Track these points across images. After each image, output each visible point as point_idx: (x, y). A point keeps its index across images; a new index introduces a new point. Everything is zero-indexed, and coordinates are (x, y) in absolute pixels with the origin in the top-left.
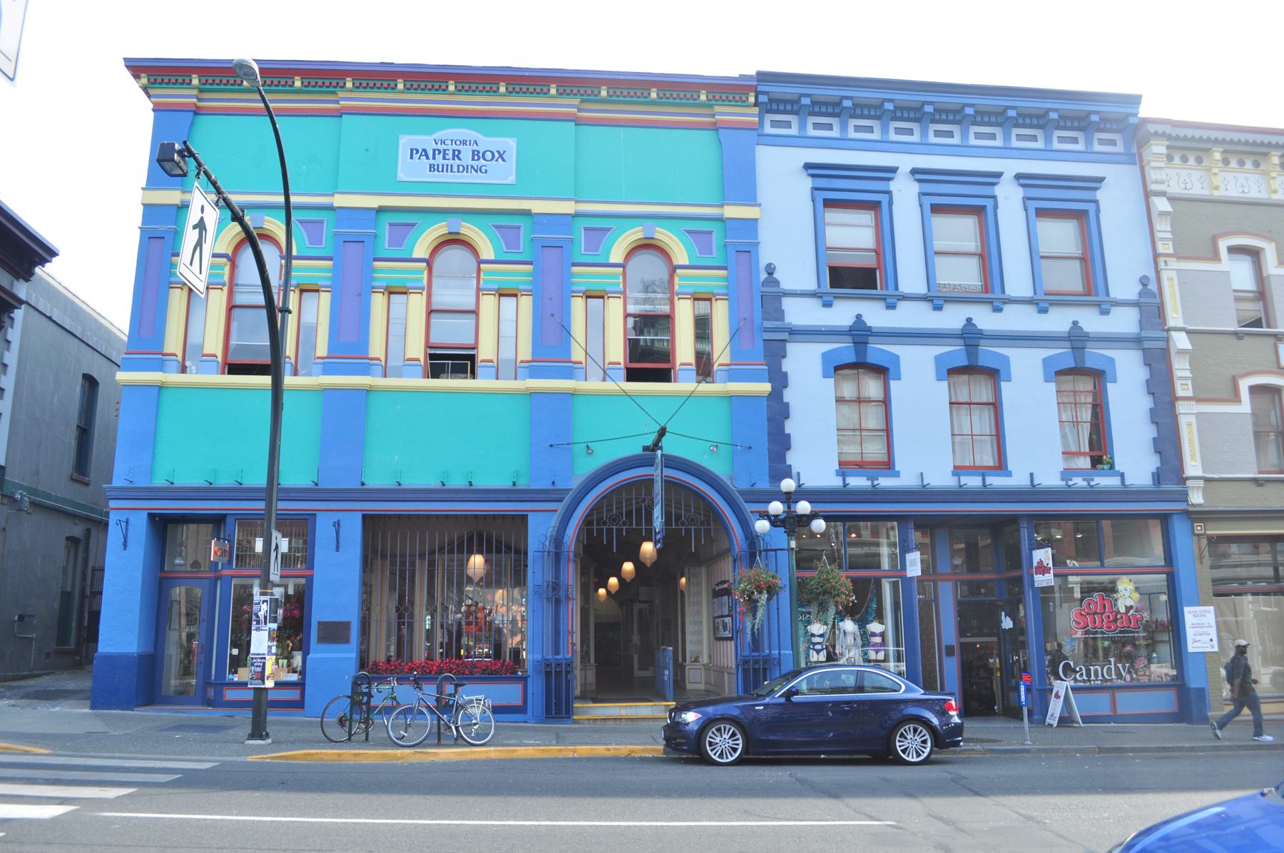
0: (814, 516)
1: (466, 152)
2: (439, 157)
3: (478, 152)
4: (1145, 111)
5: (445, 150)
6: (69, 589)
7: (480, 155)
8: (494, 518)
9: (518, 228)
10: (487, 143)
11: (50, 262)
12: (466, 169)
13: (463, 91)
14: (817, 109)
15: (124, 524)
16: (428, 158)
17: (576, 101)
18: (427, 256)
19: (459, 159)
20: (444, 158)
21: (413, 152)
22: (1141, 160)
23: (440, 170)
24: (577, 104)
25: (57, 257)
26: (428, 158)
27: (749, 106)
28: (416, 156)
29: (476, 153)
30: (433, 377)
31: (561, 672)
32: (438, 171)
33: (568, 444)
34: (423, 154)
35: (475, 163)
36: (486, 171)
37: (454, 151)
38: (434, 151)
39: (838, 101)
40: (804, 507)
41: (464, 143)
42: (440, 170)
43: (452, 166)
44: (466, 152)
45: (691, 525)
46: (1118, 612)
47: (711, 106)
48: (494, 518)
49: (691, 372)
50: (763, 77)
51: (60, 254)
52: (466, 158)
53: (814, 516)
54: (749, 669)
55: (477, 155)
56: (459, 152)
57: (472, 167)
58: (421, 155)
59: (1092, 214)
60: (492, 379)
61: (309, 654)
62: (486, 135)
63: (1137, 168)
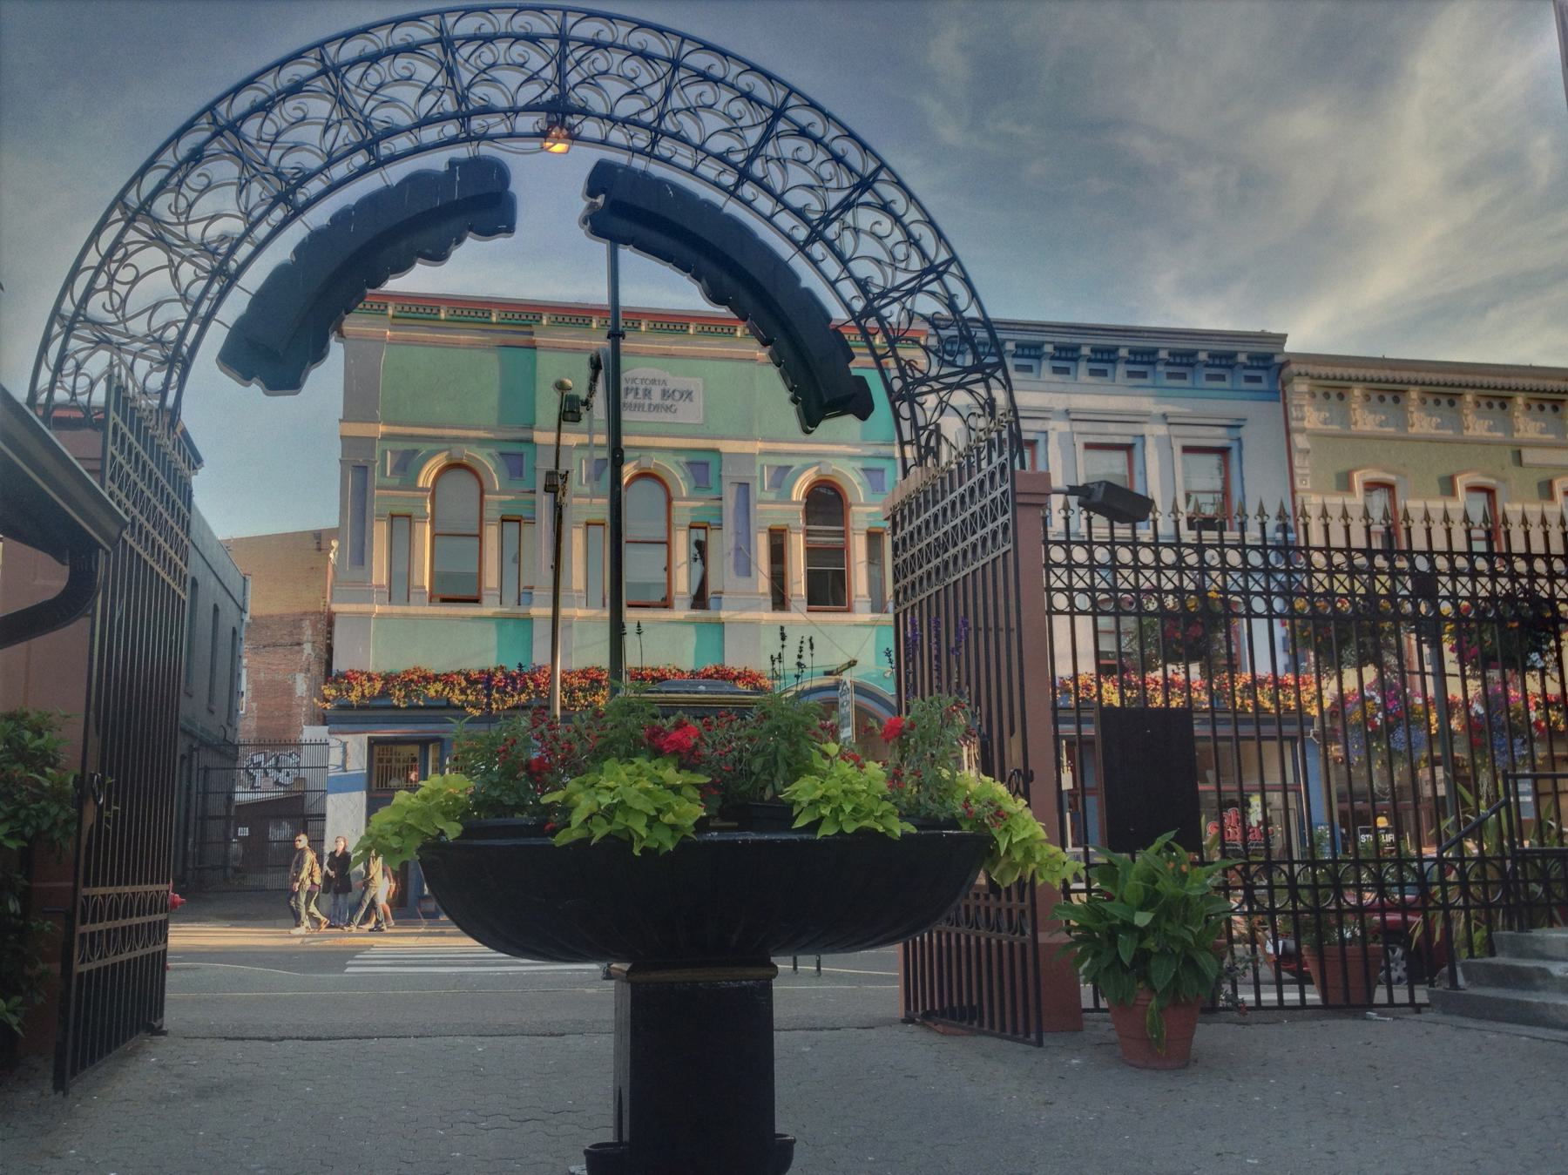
1: (656, 392)
4: (1290, 347)
9: (882, 471)
10: (674, 383)
12: (657, 408)
22: (1285, 398)
33: (783, 637)
41: (654, 381)
44: (656, 392)
46: (1251, 827)
49: (642, 536)
52: (656, 397)
59: (1041, 444)
61: (701, 818)
63: (1281, 405)
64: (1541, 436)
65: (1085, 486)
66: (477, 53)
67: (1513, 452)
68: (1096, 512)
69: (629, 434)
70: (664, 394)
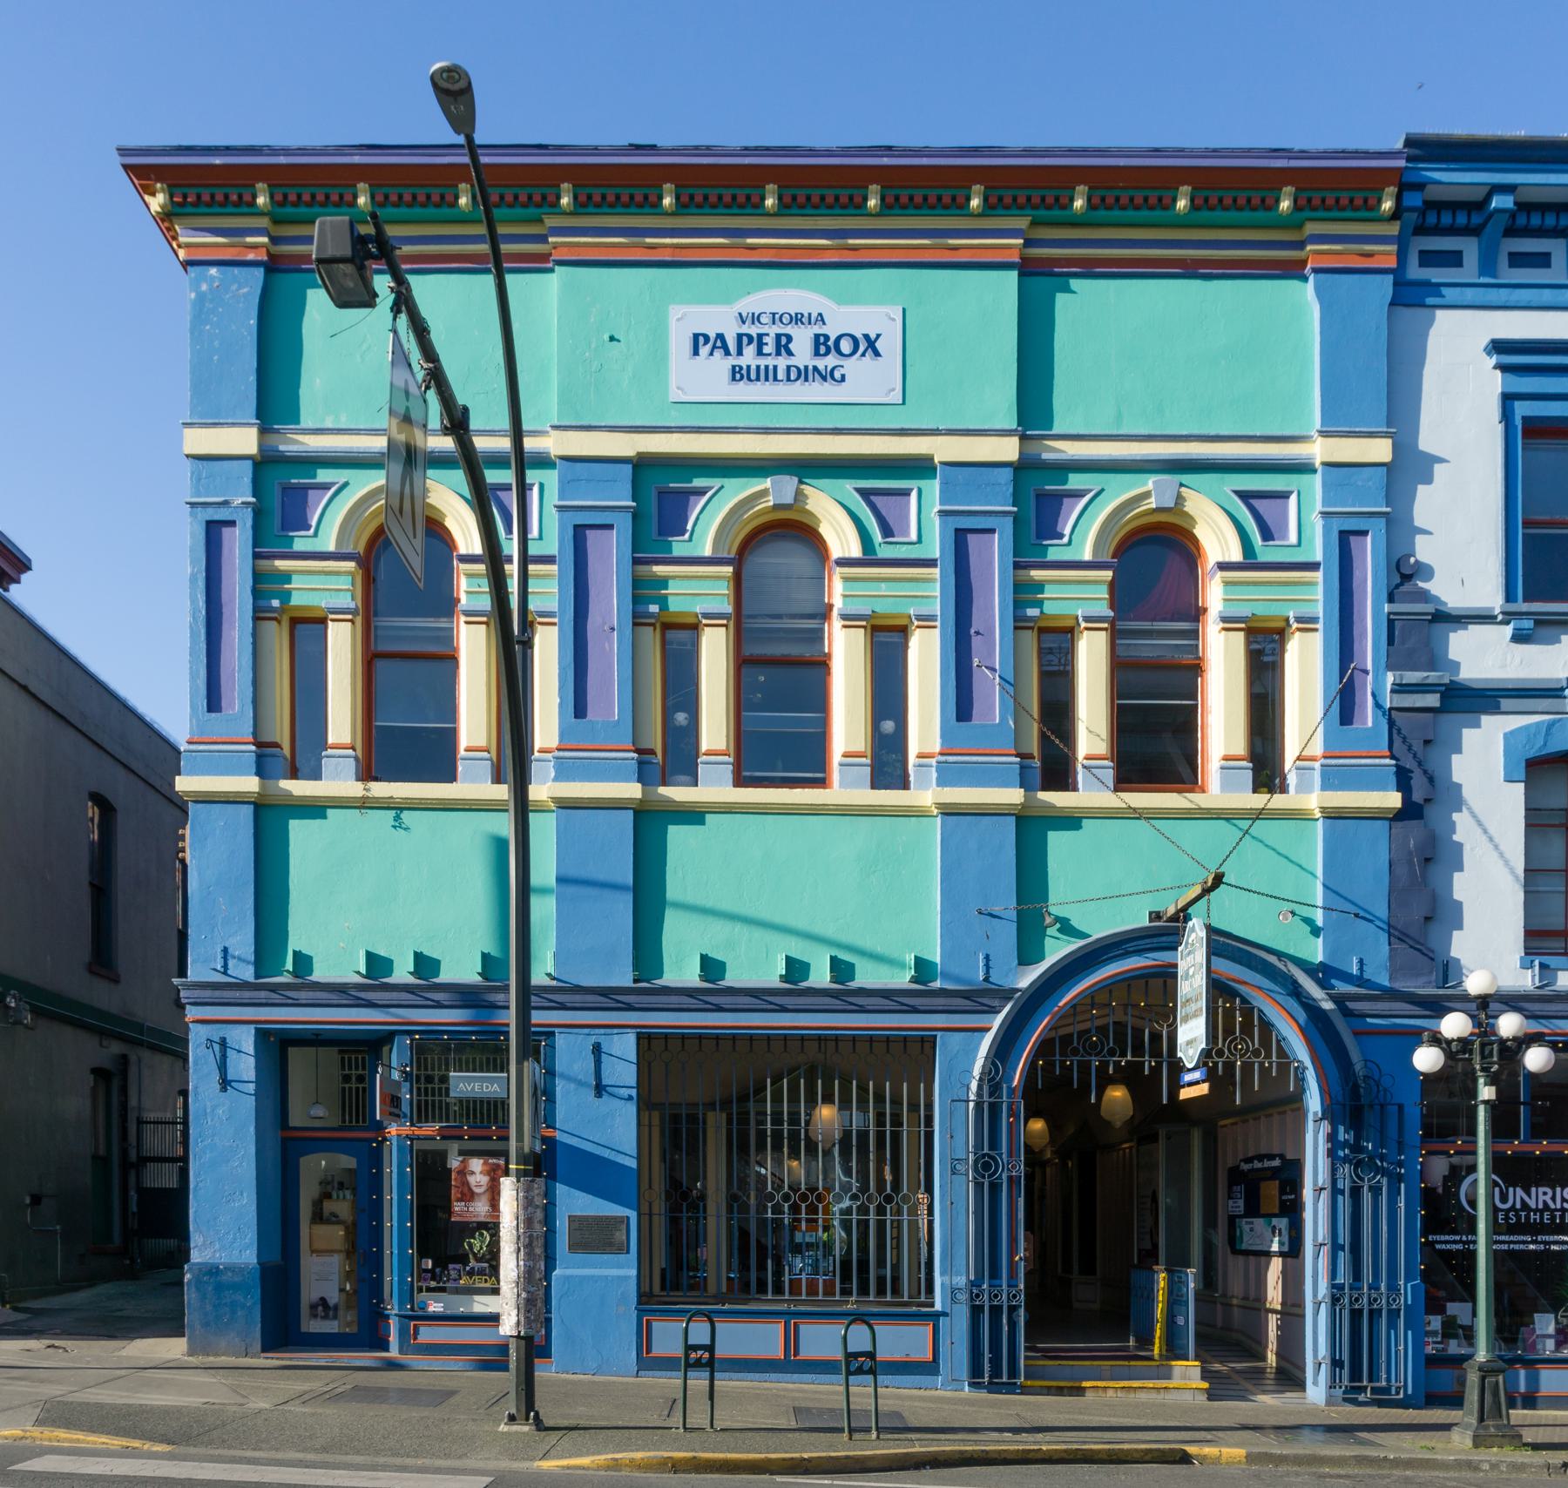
0: (1527, 1040)
1: (802, 340)
2: (750, 351)
3: (827, 338)
5: (760, 336)
6: (102, 1152)
7: (830, 343)
8: (785, 1040)
10: (843, 320)
11: (18, 581)
12: (804, 374)
13: (735, 207)
14: (1431, 219)
15: (217, 1047)
16: (727, 353)
17: (1022, 223)
18: (361, 549)
19: (790, 353)
20: (760, 353)
21: (698, 340)
23: (753, 376)
24: (1023, 227)
25: (29, 573)
26: (727, 353)
27: (1380, 220)
28: (704, 350)
29: (822, 339)
30: (873, 787)
31: (1361, 1311)
32: (749, 379)
34: (719, 344)
35: (821, 363)
36: (843, 378)
37: (778, 336)
38: (740, 336)
39: (1481, 199)
40: (1509, 1025)
41: (797, 319)
42: (753, 376)
43: (775, 368)
44: (802, 340)
45: (1090, 1055)
47: (1300, 226)
48: (785, 1040)
50: (1425, 149)
51: (34, 566)
53: (1527, 1040)
54: (1381, 1310)
55: (825, 344)
56: (789, 338)
57: (815, 368)
58: (714, 347)
60: (1015, 787)
62: (840, 302)
64: (512, 1365)
65: (488, 1173)
66: (1395, 731)
67: (1511, 265)
68: (970, 626)
69: (534, 433)
70: (821, 345)
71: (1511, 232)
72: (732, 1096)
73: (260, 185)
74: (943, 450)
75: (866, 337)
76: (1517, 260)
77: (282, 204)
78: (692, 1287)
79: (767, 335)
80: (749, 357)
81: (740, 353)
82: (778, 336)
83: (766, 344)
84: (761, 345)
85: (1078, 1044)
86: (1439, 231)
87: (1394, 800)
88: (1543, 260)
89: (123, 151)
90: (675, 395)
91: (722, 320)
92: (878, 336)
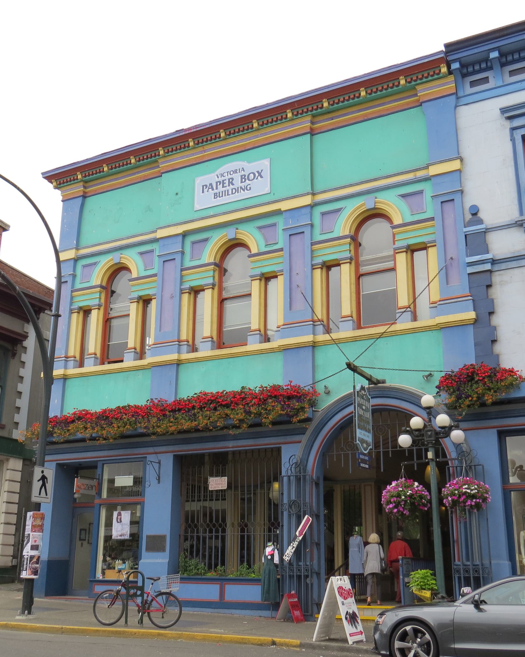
1: (237, 177)
2: (220, 187)
5: (223, 181)
19: (233, 184)
20: (223, 187)
34: (210, 187)
37: (229, 179)
38: (217, 183)
44: (237, 177)
50: (452, 48)
56: (232, 179)
57: (241, 188)
58: (209, 188)
62: (249, 162)
70: (243, 178)
71: (503, 65)
72: (234, 490)
73: (104, 165)
74: (284, 206)
75: (258, 172)
76: (473, 84)
77: (85, 176)
78: (424, 645)
79: (225, 180)
80: (220, 188)
81: (217, 188)
82: (229, 179)
83: (225, 183)
84: (223, 183)
85: (344, 446)
86: (475, 72)
87: (472, 315)
88: (486, 80)
89: (43, 174)
90: (197, 207)
91: (212, 178)
92: (262, 171)
